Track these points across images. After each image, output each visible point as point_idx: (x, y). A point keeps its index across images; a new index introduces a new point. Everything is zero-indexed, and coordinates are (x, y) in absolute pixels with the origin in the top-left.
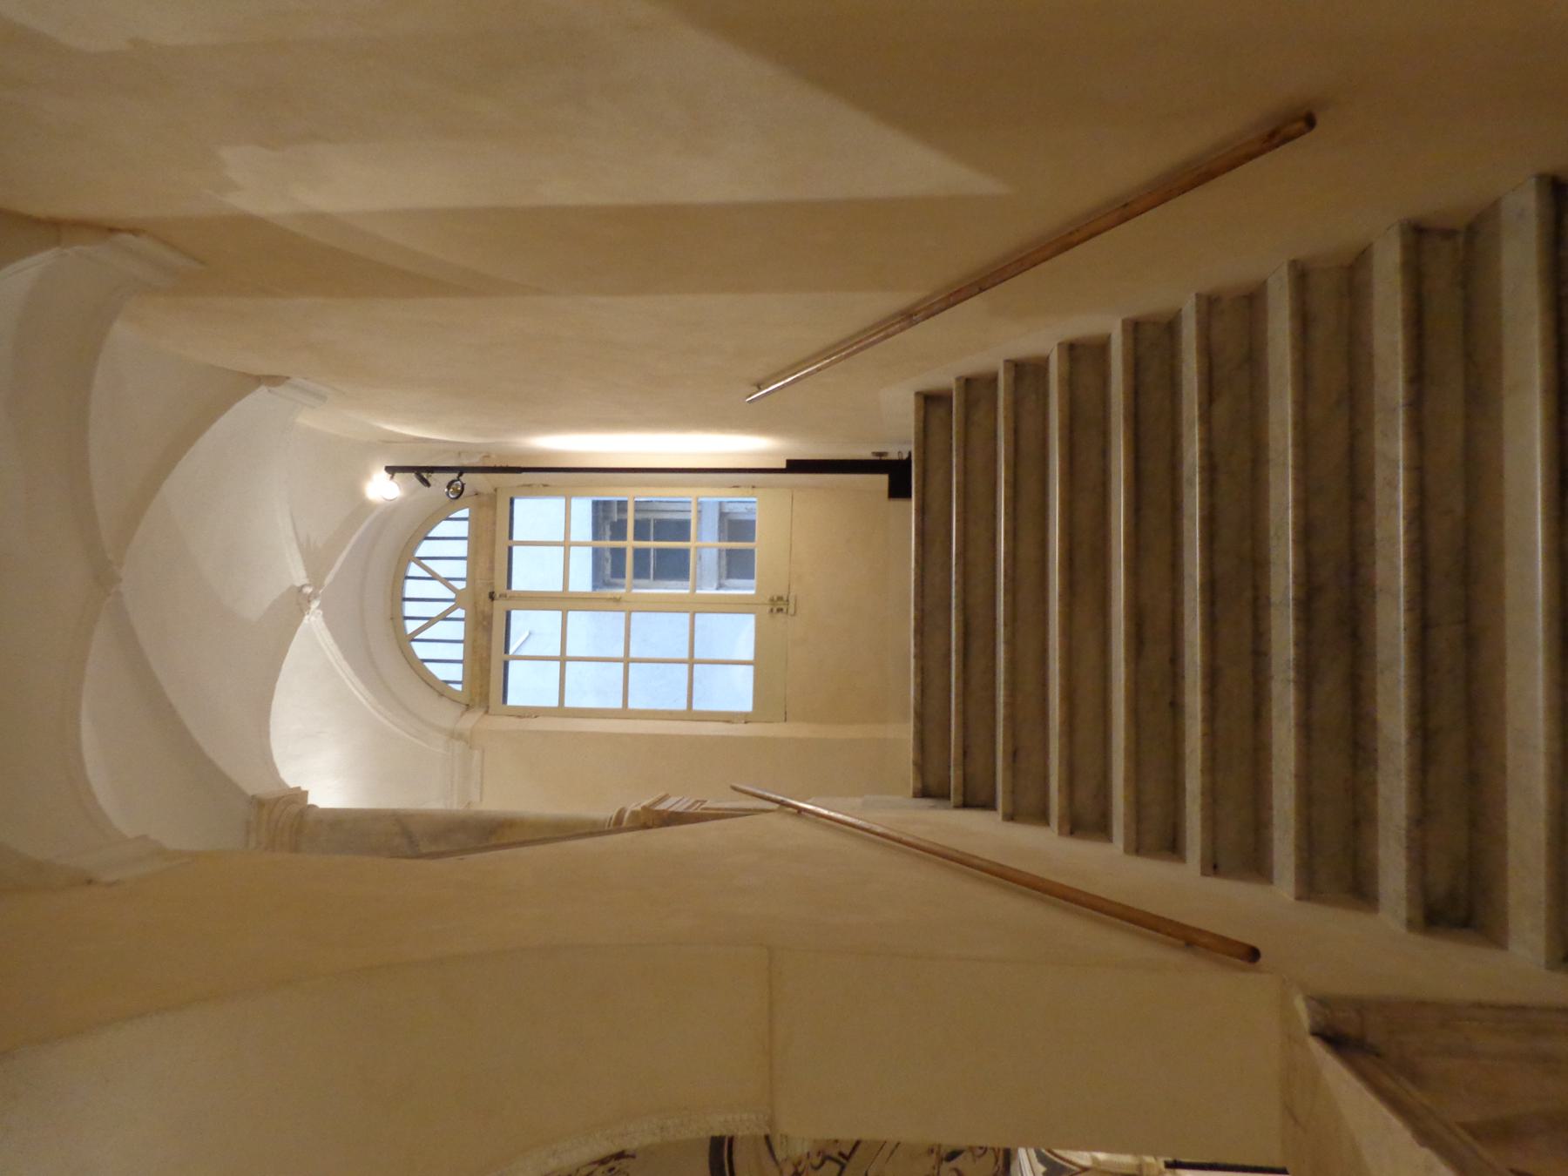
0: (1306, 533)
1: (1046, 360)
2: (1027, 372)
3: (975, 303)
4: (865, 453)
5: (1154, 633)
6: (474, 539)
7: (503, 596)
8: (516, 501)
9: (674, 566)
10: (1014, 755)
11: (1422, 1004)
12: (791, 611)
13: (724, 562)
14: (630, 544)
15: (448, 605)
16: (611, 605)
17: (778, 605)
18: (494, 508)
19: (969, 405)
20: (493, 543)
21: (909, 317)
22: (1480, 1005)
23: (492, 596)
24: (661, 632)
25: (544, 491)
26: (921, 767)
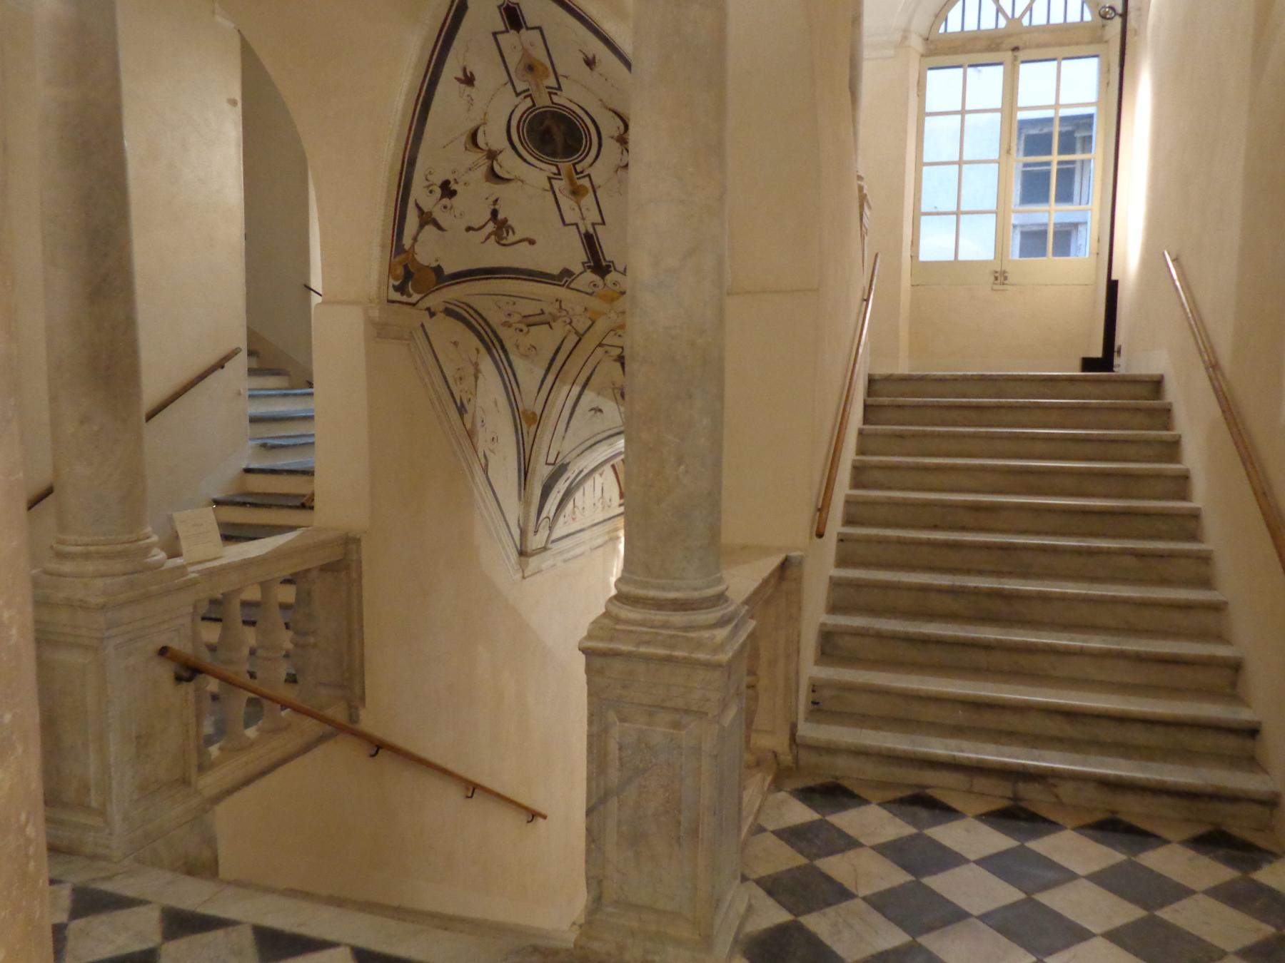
0: (1045, 598)
1: (1179, 462)
2: (1172, 449)
3: (1216, 411)
4: (1121, 338)
5: (982, 515)
6: (1065, 28)
7: (1015, 58)
8: (1095, 60)
9: (1034, 187)
10: (901, 436)
11: (800, 609)
12: (996, 287)
13: (1035, 228)
14: (1055, 158)
15: (1010, 14)
16: (1005, 147)
17: (1000, 277)
18: (1091, 43)
19: (1150, 412)
20: (1061, 45)
21: (1213, 367)
22: (799, 635)
23: (1016, 49)
24: (983, 186)
25: (1104, 83)
26: (890, 379)
